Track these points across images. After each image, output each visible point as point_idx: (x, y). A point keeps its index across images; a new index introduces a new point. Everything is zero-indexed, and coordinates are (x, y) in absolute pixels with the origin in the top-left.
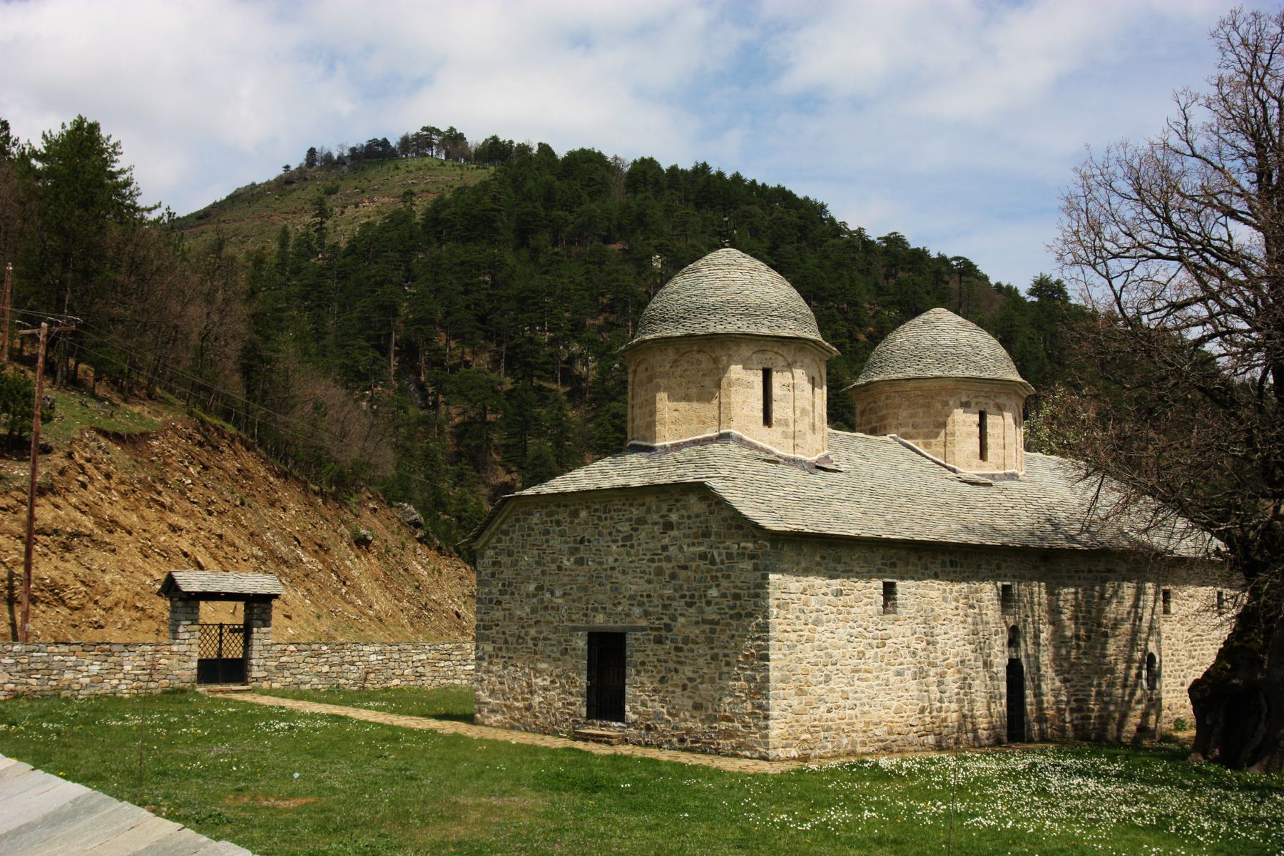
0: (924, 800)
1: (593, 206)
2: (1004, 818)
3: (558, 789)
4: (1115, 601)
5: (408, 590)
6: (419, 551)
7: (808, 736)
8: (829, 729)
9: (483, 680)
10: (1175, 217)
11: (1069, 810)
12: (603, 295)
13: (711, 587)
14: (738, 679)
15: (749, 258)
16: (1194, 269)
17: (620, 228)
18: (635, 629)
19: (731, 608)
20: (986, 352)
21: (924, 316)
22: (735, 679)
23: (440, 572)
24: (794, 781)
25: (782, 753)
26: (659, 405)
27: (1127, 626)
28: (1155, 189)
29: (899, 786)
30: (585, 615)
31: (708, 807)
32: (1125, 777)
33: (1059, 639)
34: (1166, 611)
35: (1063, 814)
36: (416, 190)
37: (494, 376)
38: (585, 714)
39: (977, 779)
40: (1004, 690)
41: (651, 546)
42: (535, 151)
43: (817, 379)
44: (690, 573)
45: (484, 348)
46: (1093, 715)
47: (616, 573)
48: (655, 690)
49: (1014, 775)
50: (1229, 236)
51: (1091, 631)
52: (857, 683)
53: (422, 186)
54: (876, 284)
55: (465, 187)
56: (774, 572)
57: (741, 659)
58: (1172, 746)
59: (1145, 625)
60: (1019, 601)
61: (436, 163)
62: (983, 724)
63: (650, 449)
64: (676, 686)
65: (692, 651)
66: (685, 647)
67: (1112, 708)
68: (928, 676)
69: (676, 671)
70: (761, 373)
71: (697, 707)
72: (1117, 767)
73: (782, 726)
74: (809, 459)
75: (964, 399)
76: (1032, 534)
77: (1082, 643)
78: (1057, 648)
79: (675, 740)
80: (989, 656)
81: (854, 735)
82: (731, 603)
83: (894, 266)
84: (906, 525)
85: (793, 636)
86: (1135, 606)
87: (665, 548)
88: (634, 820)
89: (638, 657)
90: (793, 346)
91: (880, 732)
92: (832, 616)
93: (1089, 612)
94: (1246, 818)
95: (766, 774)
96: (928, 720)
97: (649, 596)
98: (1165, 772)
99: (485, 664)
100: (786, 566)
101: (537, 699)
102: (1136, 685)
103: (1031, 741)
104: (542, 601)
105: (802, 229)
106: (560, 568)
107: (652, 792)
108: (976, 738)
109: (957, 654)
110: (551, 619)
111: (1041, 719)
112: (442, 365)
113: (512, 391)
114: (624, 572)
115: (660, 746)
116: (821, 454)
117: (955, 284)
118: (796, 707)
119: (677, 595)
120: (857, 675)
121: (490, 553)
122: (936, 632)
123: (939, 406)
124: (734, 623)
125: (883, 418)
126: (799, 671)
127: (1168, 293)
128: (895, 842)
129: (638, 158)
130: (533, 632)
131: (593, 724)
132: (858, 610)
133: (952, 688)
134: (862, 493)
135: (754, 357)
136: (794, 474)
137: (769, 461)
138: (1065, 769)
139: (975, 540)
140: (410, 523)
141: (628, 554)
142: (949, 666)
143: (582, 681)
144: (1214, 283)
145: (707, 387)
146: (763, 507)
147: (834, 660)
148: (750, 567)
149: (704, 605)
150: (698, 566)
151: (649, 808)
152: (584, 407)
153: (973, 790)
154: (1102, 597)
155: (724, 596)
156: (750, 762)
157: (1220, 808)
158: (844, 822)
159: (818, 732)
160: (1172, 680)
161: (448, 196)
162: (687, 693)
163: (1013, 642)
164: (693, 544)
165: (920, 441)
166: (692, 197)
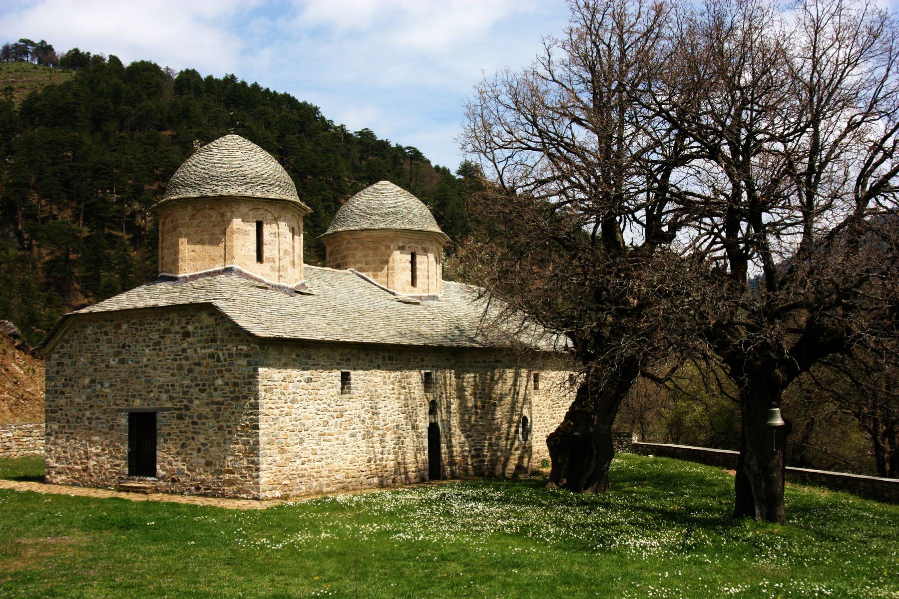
0: (365, 524)
1: (150, 103)
2: (418, 533)
3: (100, 529)
4: (501, 382)
5: (8, 385)
6: (17, 356)
7: (288, 482)
8: (304, 476)
9: (51, 450)
10: (539, 122)
11: (463, 525)
12: (157, 168)
13: (217, 378)
14: (237, 443)
15: (248, 142)
16: (551, 156)
17: (170, 119)
18: (163, 410)
19: (232, 393)
20: (416, 212)
21: (375, 186)
22: (236, 444)
23: (34, 371)
24: (275, 514)
25: (269, 495)
26: (181, 247)
27: (509, 398)
28: (528, 103)
29: (349, 514)
30: (127, 400)
31: (210, 536)
32: (504, 500)
33: (464, 409)
34: (536, 388)
35: (458, 528)
36: (15, 86)
37: (74, 226)
38: (127, 473)
39: (403, 507)
40: (426, 444)
41: (174, 349)
42: (107, 61)
43: (296, 229)
44: (202, 368)
45: (67, 206)
46: (487, 459)
47: (149, 370)
48: (178, 453)
49: (429, 503)
50: (573, 135)
51: (485, 403)
52: (323, 443)
53: (20, 84)
54: (353, 164)
55: (53, 86)
56: (262, 366)
57: (239, 429)
58: (537, 478)
59: (521, 397)
60: (436, 383)
61: (30, 67)
62: (412, 468)
63: (175, 279)
64: (193, 449)
65: (204, 424)
66: (199, 422)
67: (499, 454)
68: (373, 436)
69: (193, 439)
70: (255, 224)
71: (209, 464)
72: (498, 494)
73: (269, 475)
74: (290, 286)
75: (401, 244)
76: (446, 337)
77: (479, 411)
78: (462, 415)
79: (193, 488)
80: (416, 421)
81: (321, 479)
82: (232, 389)
83: (365, 152)
84: (358, 332)
85: (277, 412)
86: (514, 385)
87: (184, 350)
88: (153, 548)
89: (166, 430)
90: (278, 206)
91: (340, 476)
92: (305, 397)
93: (484, 390)
94: (578, 524)
95: (255, 510)
96: (373, 467)
97: (173, 385)
98: (531, 496)
99: (52, 438)
100: (271, 362)
101: (92, 463)
102: (515, 438)
103: (445, 478)
104: (94, 391)
105: (302, 124)
106: (107, 367)
107: (172, 526)
108: (407, 478)
109: (394, 421)
110: (101, 404)
111: (452, 463)
112: (35, 217)
113: (89, 237)
114: (155, 369)
115: (182, 494)
116: (299, 283)
117: (405, 167)
118: (279, 461)
119: (193, 384)
120: (323, 438)
121: (55, 356)
122: (378, 406)
123: (383, 249)
124: (234, 403)
125: (344, 257)
126: (281, 436)
127: (534, 173)
128: (340, 554)
129: (184, 69)
130: (88, 414)
131: (134, 480)
132: (323, 392)
133: (390, 443)
134: (327, 309)
135: (250, 213)
136: (279, 297)
137: (260, 287)
138: (464, 497)
139: (406, 342)
140: (10, 335)
141: (158, 355)
142: (388, 429)
143: (125, 448)
144: (565, 166)
145: (216, 235)
146: (255, 320)
147: (306, 427)
148: (245, 363)
149: (212, 391)
150: (208, 363)
151: (166, 539)
152: (143, 249)
153: (400, 515)
154: (492, 379)
155: (227, 384)
156: (245, 502)
157: (562, 519)
158: (306, 542)
159: (295, 479)
160: (540, 434)
161: (40, 92)
162: (201, 454)
163: (432, 411)
164: (205, 348)
165: (370, 273)
166: (223, 99)
